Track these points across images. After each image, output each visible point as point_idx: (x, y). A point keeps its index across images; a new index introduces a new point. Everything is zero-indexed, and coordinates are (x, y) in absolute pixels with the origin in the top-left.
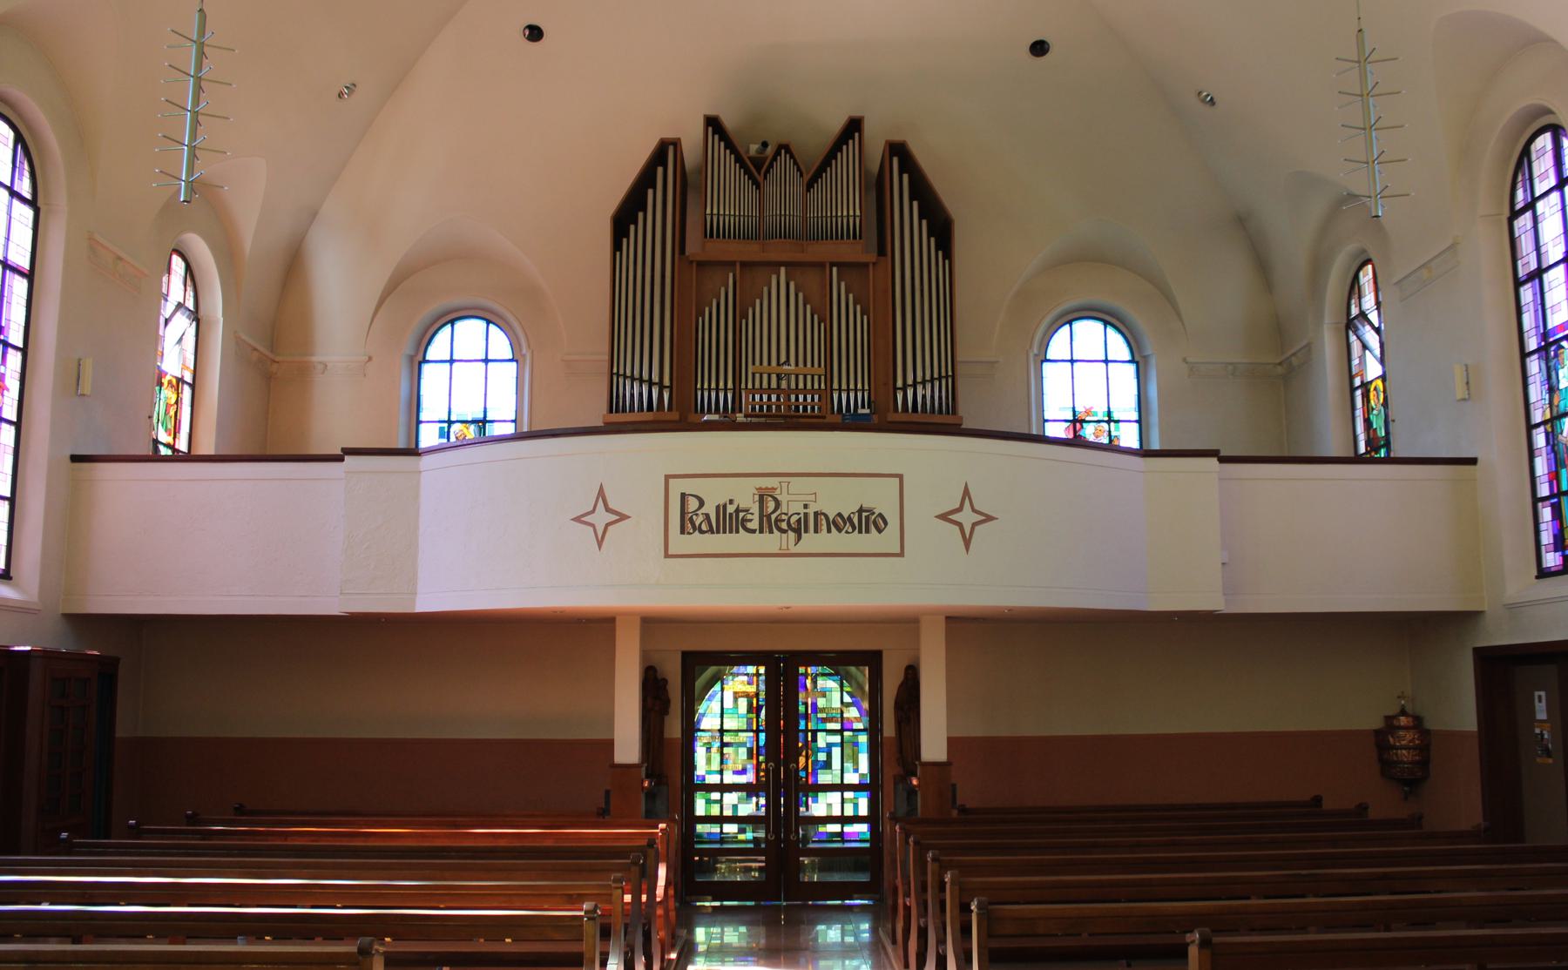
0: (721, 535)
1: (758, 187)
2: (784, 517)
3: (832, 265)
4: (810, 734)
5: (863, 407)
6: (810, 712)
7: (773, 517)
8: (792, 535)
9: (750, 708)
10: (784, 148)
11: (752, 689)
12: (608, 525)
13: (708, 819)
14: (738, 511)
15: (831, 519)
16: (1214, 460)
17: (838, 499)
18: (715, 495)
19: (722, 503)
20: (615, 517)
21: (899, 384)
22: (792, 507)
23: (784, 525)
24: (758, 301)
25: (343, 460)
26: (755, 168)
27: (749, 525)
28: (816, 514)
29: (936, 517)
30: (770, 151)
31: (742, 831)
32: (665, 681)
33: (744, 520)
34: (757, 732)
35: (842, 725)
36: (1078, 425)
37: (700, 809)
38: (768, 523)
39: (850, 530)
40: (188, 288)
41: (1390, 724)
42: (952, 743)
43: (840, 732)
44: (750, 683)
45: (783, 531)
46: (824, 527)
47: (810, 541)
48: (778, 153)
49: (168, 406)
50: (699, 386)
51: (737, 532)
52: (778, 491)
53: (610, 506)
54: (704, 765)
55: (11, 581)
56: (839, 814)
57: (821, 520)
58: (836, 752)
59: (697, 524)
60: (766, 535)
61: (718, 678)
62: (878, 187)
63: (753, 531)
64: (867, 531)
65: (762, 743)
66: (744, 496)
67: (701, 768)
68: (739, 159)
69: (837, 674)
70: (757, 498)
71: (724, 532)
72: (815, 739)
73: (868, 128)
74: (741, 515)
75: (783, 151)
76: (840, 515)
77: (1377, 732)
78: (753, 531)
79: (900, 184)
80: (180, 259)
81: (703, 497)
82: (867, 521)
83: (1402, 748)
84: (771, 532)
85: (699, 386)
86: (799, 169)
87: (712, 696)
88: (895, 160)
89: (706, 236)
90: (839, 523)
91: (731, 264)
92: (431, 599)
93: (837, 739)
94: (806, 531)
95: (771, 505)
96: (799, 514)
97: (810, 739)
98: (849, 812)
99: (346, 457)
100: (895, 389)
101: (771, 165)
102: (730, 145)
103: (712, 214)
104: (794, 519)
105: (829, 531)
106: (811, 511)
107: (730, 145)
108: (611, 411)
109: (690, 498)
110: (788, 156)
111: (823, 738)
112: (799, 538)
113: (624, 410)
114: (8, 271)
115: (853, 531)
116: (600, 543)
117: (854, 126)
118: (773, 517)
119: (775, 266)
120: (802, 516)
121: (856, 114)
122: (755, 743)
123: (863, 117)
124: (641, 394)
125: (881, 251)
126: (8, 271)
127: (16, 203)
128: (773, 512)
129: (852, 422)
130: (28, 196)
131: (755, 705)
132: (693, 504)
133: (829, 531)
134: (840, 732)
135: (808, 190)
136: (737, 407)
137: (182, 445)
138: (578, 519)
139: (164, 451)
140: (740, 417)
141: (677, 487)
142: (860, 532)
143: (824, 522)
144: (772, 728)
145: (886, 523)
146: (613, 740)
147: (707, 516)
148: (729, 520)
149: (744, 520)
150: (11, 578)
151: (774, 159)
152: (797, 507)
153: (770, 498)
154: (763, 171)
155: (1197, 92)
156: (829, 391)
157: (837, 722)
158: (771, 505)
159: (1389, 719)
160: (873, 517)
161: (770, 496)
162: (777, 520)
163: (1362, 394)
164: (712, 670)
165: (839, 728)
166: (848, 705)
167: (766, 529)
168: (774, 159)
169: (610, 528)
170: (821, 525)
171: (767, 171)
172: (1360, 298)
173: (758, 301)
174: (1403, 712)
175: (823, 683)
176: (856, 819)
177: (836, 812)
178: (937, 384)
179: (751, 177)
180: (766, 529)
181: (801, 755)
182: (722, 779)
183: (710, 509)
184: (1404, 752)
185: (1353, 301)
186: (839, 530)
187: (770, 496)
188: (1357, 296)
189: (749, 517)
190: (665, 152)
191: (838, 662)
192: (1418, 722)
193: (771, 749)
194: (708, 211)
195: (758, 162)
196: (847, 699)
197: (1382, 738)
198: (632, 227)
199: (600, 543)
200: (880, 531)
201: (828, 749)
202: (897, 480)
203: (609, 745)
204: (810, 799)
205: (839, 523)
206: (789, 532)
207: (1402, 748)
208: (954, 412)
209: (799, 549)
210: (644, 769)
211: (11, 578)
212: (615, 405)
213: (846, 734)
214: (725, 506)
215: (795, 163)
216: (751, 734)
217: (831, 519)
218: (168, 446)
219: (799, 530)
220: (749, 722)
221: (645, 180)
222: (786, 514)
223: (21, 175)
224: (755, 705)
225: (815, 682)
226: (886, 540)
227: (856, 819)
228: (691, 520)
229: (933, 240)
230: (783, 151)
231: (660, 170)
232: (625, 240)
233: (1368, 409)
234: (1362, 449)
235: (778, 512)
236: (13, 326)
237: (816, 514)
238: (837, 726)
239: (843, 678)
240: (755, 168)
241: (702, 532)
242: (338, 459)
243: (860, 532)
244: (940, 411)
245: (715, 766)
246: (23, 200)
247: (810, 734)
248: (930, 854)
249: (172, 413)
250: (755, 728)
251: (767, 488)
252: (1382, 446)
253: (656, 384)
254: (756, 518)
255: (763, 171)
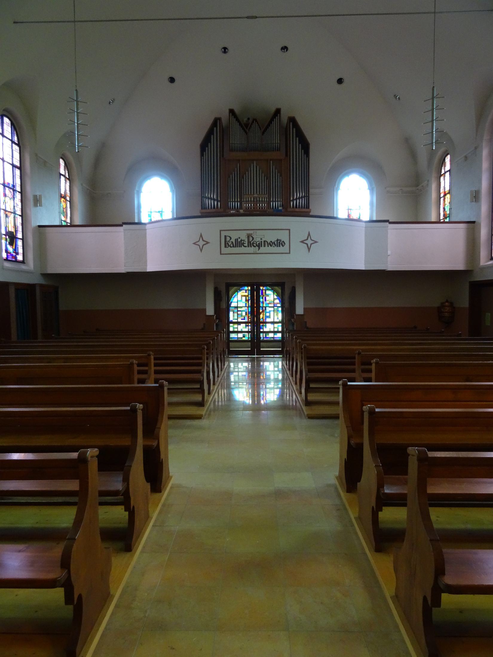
0: (237, 248)
1: (247, 134)
2: (255, 242)
3: (270, 160)
4: (264, 308)
5: (280, 207)
6: (264, 301)
7: (252, 242)
8: (257, 247)
9: (246, 300)
10: (255, 120)
11: (247, 294)
12: (199, 241)
13: (234, 332)
14: (241, 240)
15: (269, 243)
16: (388, 223)
17: (271, 237)
18: (234, 236)
19: (236, 238)
20: (205, 243)
21: (292, 199)
22: (257, 239)
23: (255, 245)
24: (247, 173)
25: (122, 226)
26: (246, 127)
27: (245, 245)
28: (264, 241)
29: (300, 242)
30: (251, 121)
31: (244, 336)
32: (220, 291)
33: (243, 243)
34: (248, 307)
35: (274, 305)
36: (349, 211)
37: (231, 329)
38: (250, 244)
39: (274, 246)
40: (66, 170)
41: (443, 305)
42: (305, 309)
43: (273, 307)
44: (246, 292)
45: (254, 246)
46: (267, 245)
47: (263, 249)
48: (253, 122)
49: (64, 208)
50: (229, 200)
51: (241, 247)
52: (253, 235)
53: (204, 240)
54: (232, 317)
55: (25, 264)
56: (273, 330)
57: (266, 243)
58: (272, 313)
59: (229, 245)
60: (250, 248)
61: (237, 291)
62: (285, 132)
63: (246, 247)
64: (279, 246)
65: (250, 310)
66: (243, 236)
67: (231, 318)
68: (240, 124)
69: (272, 289)
70: (247, 237)
71: (238, 247)
72: (266, 309)
73: (282, 112)
74: (242, 242)
75: (255, 121)
76: (271, 242)
77: (438, 307)
78: (246, 247)
79: (292, 132)
80: (62, 160)
81: (232, 237)
82: (279, 243)
83: (446, 312)
84: (251, 247)
85: (229, 200)
86: (260, 128)
87: (235, 295)
88: (291, 124)
89: (230, 151)
90: (271, 244)
91: (239, 160)
92: (151, 267)
93: (272, 309)
94: (261, 246)
95: (251, 239)
96: (259, 241)
97: (264, 309)
98: (276, 330)
99: (124, 225)
100: (290, 201)
101: (251, 126)
102: (237, 120)
103: (232, 143)
104: (258, 243)
105: (268, 246)
106: (263, 241)
107: (237, 120)
108: (202, 209)
109: (227, 237)
110: (256, 123)
111: (268, 309)
112: (259, 249)
113: (206, 209)
114: (14, 168)
115: (275, 246)
116: (201, 250)
117: (278, 111)
118: (252, 242)
119: (253, 160)
120: (260, 242)
121: (279, 107)
122: (248, 310)
123: (281, 108)
124: (211, 203)
125: (286, 155)
126: (14, 168)
127: (14, 145)
128: (252, 241)
129: (276, 213)
130: (17, 142)
131: (247, 299)
132: (228, 239)
133: (268, 246)
134: (273, 307)
135: (263, 134)
136: (241, 207)
137: (69, 221)
138: (194, 243)
139: (64, 224)
140: (241, 211)
141: (223, 234)
142: (277, 246)
143: (267, 244)
144: (252, 306)
145: (285, 244)
146: (206, 309)
147: (232, 242)
148: (239, 243)
149: (243, 243)
150: (25, 263)
151: (252, 124)
152: (259, 239)
153: (251, 237)
154: (248, 128)
155: (394, 95)
156: (269, 202)
157: (272, 304)
158: (251, 239)
159: (442, 304)
160: (281, 242)
161: (251, 236)
162: (253, 243)
163: (443, 199)
164: (235, 288)
165: (273, 306)
166: (276, 299)
167: (250, 246)
168: (252, 124)
169: (204, 246)
170: (266, 245)
171: (250, 128)
172: (445, 167)
173: (247, 173)
174: (447, 301)
175: (268, 292)
176: (278, 332)
177: (272, 330)
178: (306, 198)
179: (243, 129)
180: (250, 246)
181: (261, 314)
182: (238, 330)
183: (233, 240)
184: (446, 313)
185: (443, 168)
186: (271, 246)
187: (251, 236)
188: (444, 166)
189: (245, 242)
190: (216, 122)
191: (272, 286)
192: (452, 304)
193: (252, 312)
194: (231, 142)
195: (247, 125)
196: (275, 297)
197: (439, 310)
198: (207, 148)
199: (201, 250)
200: (283, 246)
201: (269, 312)
202: (288, 231)
203: (204, 310)
204: (264, 327)
205: (271, 244)
206: (257, 247)
207: (446, 312)
208: (309, 208)
209: (259, 252)
210: (215, 317)
211: (25, 263)
212: (203, 207)
213: (275, 308)
214: (237, 239)
215: (259, 125)
216: (246, 308)
217: (269, 243)
218: (65, 221)
219: (259, 246)
220: (246, 304)
221: (210, 132)
222: (255, 241)
223: (14, 134)
224: (247, 299)
225: (265, 292)
226: (285, 249)
227: (278, 332)
228: (228, 243)
229: (303, 151)
230: (255, 121)
231: (215, 128)
232: (205, 153)
233: (444, 205)
234: (442, 217)
235: (253, 241)
236: (17, 185)
237: (264, 241)
238: (273, 305)
239: (274, 291)
240: (246, 127)
241: (231, 247)
242: (121, 225)
243: (277, 246)
244: (304, 208)
245: (236, 317)
246: (16, 144)
247: (264, 308)
248: (294, 337)
249: (65, 211)
250: (247, 306)
251: (250, 234)
252: (448, 217)
253: (216, 200)
254: (247, 243)
255: (248, 128)
